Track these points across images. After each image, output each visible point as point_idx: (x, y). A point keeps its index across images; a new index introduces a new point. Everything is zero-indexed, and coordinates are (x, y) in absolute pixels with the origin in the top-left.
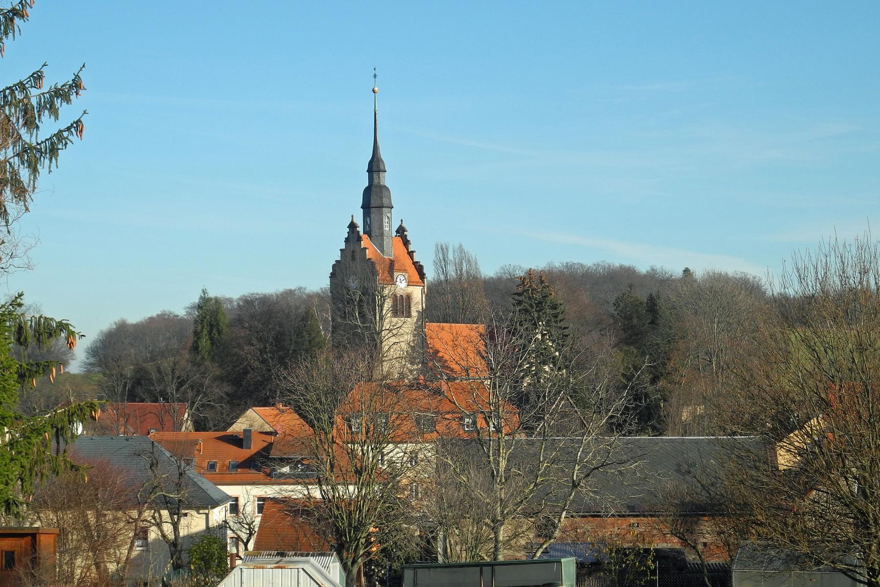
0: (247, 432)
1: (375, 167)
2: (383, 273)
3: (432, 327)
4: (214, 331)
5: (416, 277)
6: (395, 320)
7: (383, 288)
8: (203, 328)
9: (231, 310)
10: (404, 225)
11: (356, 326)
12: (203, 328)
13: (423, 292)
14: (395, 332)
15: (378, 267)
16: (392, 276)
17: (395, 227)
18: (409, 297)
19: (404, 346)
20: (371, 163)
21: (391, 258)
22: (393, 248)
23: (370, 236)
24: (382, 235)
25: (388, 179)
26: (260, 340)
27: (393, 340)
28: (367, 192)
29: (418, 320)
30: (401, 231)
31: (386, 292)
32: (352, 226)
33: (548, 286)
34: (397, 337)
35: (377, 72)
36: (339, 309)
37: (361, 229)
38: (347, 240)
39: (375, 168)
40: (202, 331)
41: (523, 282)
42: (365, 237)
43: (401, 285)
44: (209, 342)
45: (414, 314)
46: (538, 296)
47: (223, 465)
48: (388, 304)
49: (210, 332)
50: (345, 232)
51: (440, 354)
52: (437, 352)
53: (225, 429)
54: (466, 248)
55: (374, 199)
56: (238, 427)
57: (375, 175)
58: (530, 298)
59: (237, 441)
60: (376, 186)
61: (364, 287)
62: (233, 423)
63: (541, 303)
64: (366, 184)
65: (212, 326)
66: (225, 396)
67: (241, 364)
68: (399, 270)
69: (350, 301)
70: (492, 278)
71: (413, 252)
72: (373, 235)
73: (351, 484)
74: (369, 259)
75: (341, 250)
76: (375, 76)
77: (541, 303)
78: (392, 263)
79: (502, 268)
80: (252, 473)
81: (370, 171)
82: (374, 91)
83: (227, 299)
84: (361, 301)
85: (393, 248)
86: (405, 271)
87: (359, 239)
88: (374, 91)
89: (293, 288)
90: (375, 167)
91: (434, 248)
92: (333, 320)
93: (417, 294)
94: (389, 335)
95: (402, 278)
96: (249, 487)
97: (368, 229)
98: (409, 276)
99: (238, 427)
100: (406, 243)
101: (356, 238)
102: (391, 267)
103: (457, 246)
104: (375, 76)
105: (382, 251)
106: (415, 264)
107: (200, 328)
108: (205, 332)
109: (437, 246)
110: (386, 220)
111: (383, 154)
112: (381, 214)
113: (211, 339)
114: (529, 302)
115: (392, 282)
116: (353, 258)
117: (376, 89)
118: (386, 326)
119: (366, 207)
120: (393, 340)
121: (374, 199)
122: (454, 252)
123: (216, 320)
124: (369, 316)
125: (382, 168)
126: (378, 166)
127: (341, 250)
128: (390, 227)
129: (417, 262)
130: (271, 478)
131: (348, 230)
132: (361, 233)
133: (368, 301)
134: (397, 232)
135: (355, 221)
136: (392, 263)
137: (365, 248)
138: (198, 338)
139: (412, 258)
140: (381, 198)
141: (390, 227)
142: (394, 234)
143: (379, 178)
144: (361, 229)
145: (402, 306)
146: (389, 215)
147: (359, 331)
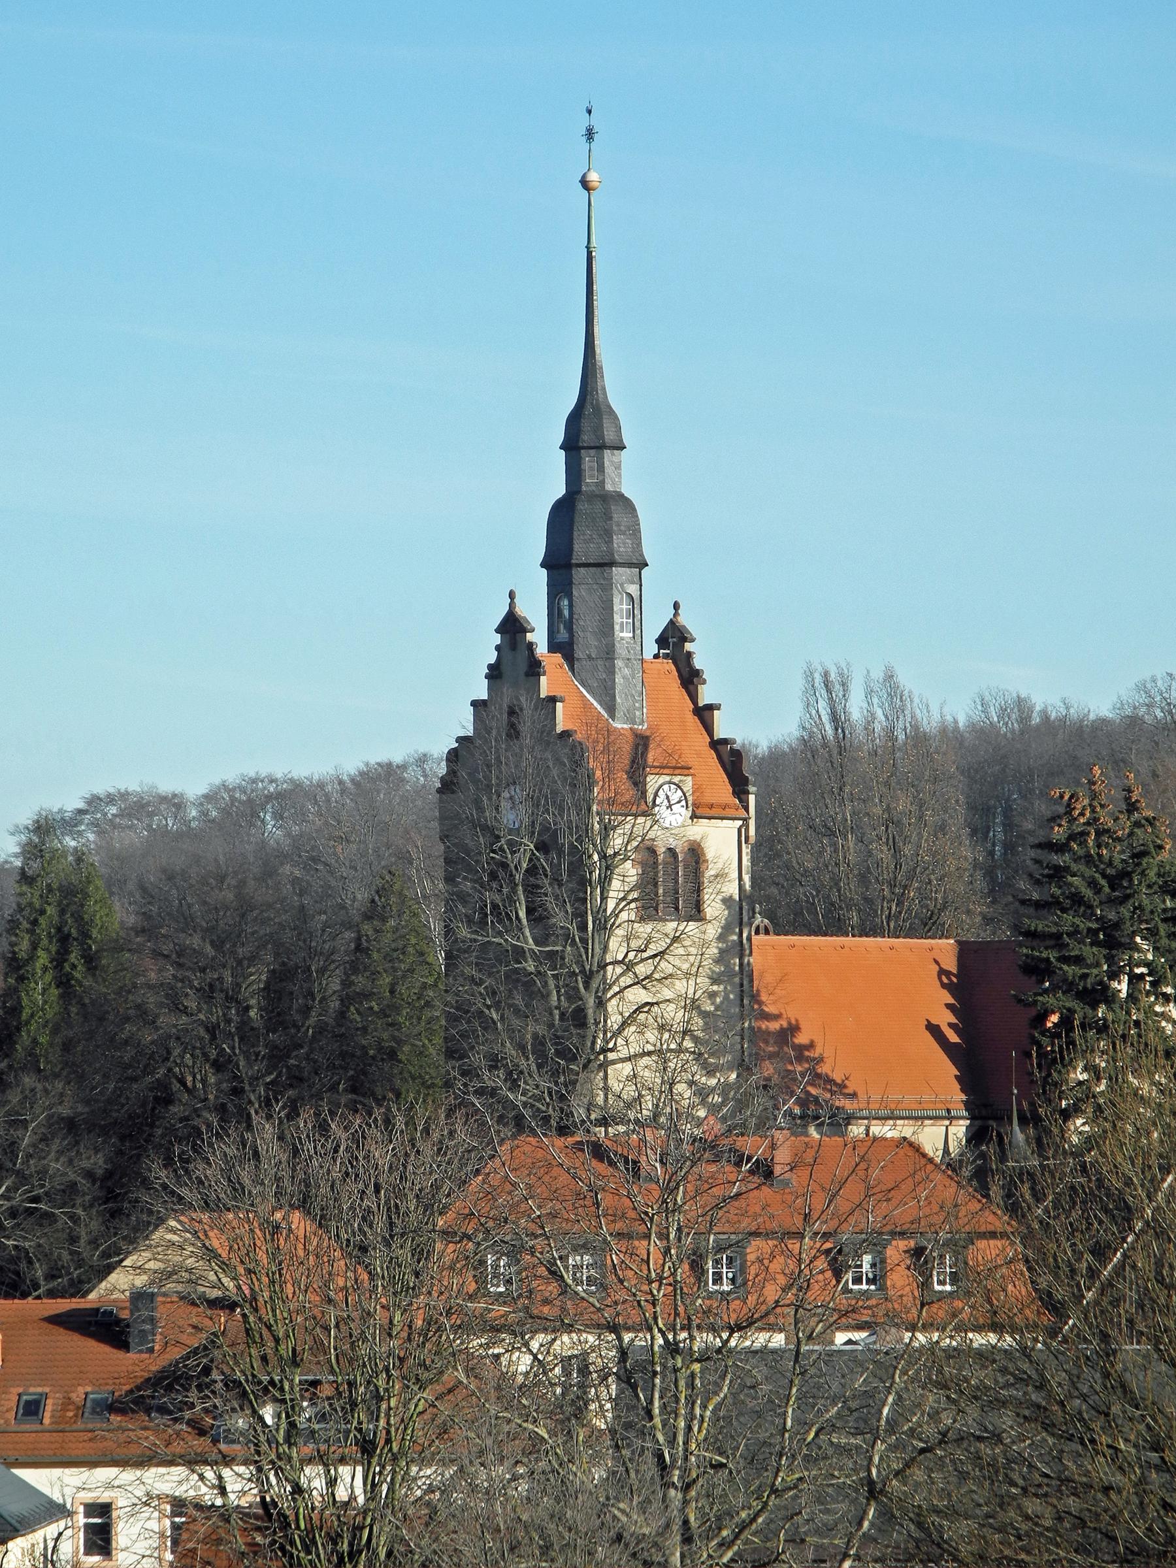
0: (140, 1298)
1: (588, 432)
2: (609, 776)
3: (769, 951)
4: (73, 957)
5: (723, 790)
6: (645, 929)
7: (607, 829)
8: (34, 946)
9: (179, 836)
10: (684, 620)
11: (519, 954)
12: (34, 946)
13: (742, 836)
14: (642, 970)
15: (594, 764)
16: (639, 784)
17: (654, 627)
18: (696, 853)
19: (674, 1014)
20: (575, 420)
21: (642, 728)
22: (643, 697)
23: (570, 659)
24: (609, 654)
25: (628, 473)
26: (208, 993)
27: (638, 995)
28: (563, 516)
29: (727, 929)
30: (674, 639)
31: (617, 841)
32: (512, 627)
33: (1151, 821)
34: (656, 989)
35: (596, 121)
36: (463, 898)
37: (539, 638)
38: (495, 673)
39: (586, 438)
40: (32, 958)
41: (1069, 809)
42: (552, 662)
43: (673, 822)
44: (55, 992)
45: (713, 908)
46: (1118, 855)
47: (68, 1402)
48: (629, 873)
49: (59, 961)
50: (486, 647)
51: (801, 1039)
52: (794, 1029)
53: (78, 1288)
54: (905, 680)
55: (584, 538)
56: (118, 1286)
57: (588, 461)
58: (1088, 859)
59: (108, 1329)
60: (592, 497)
61: (545, 829)
62: (110, 1269)
63: (1126, 874)
64: (560, 490)
65: (64, 940)
66: (83, 1183)
67: (145, 1072)
68: (662, 769)
69: (500, 871)
70: (1104, 721)
71: (710, 708)
72: (579, 653)
73: (343, 1460)
74: (566, 734)
75: (475, 704)
76: (590, 134)
77: (1126, 874)
78: (642, 743)
79: (1142, 687)
80: (144, 1432)
81: (572, 446)
82: (585, 184)
83: (164, 799)
84: (532, 870)
85: (643, 697)
86: (684, 769)
87: (534, 668)
88: (585, 184)
89: (398, 758)
90: (588, 432)
91: (800, 683)
92: (448, 931)
93: (723, 844)
94: (626, 980)
95: (676, 796)
96: (57, 1472)
97: (563, 635)
98: (696, 789)
99: (118, 1286)
100: (690, 678)
101: (523, 666)
102: (639, 757)
103: (878, 674)
104: (590, 134)
105: (611, 710)
106: (717, 745)
107: (25, 945)
108: (43, 958)
109: (809, 675)
110: (620, 606)
111: (616, 390)
112: (607, 588)
113: (64, 982)
114: (1089, 872)
115: (643, 806)
116: (513, 732)
117: (593, 177)
118: (616, 948)
119: (559, 563)
120: (638, 995)
121: (584, 538)
122: (869, 693)
123: (78, 918)
124: (561, 919)
125: (609, 436)
126: (598, 429)
127: (475, 704)
128: (637, 636)
129: (725, 741)
130: (206, 1447)
131: (497, 639)
132: (542, 649)
133: (564, 869)
134: (662, 641)
135: (522, 610)
136: (642, 743)
137: (553, 700)
138: (21, 979)
139: (709, 728)
140: (608, 535)
141: (637, 628)
142: (651, 648)
143: (601, 468)
144: (539, 638)
145: (674, 884)
146: (633, 589)
147: (530, 966)
